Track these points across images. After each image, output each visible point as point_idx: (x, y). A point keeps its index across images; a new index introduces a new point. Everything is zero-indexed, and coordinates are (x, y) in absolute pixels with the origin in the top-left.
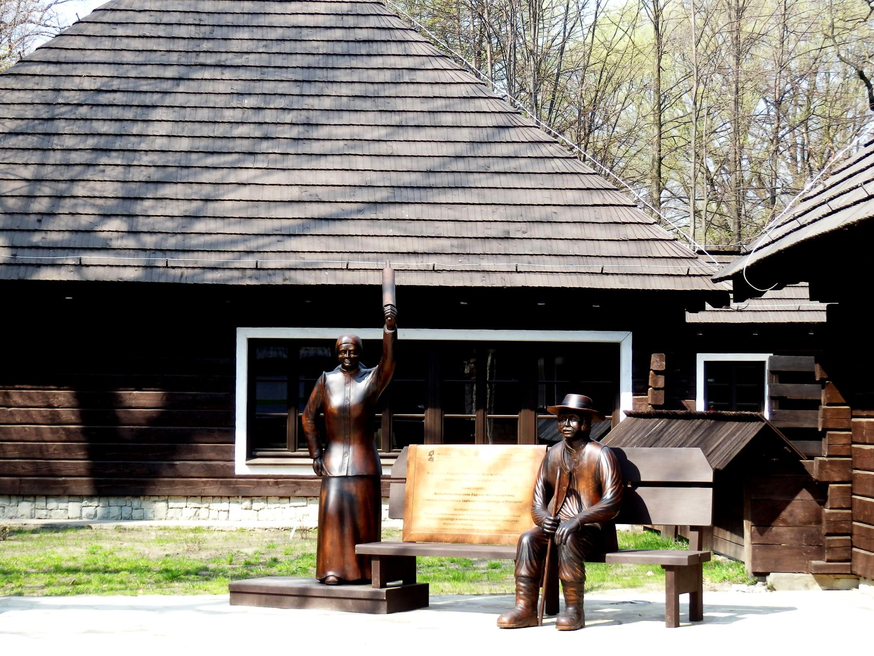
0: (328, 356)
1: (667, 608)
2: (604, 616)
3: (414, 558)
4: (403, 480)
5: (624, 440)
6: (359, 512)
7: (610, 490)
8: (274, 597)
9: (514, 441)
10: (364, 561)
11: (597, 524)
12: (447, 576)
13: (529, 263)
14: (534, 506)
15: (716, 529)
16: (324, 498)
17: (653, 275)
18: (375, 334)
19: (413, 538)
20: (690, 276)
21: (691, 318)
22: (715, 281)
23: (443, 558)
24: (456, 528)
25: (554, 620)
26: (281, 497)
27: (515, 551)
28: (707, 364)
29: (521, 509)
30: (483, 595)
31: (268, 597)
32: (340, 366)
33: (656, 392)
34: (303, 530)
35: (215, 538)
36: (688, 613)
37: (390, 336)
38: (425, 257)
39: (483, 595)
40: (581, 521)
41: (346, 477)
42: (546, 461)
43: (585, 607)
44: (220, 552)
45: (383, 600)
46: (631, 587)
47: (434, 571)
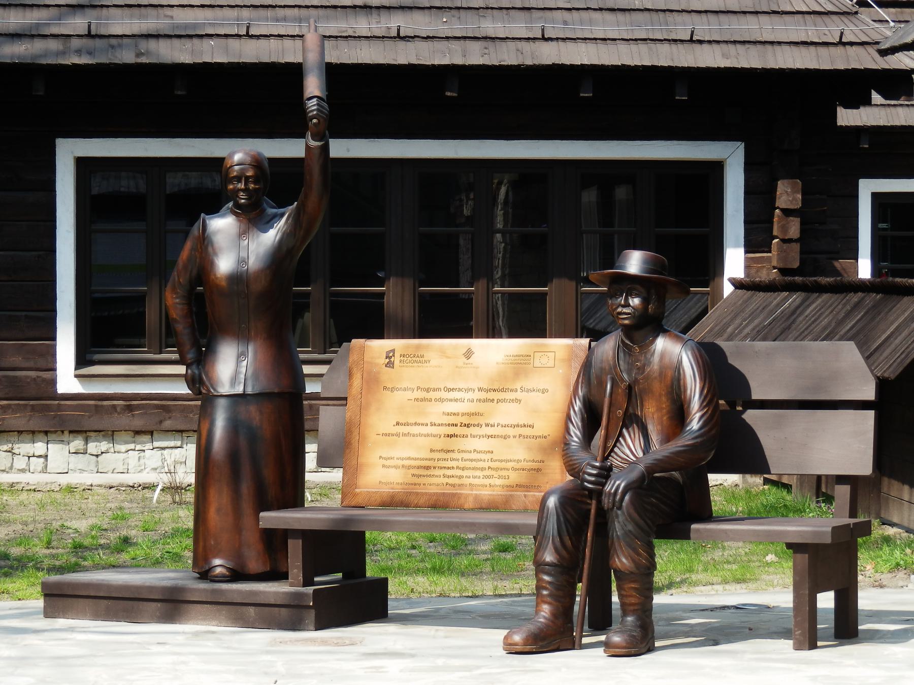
0: (207, 189)
1: (795, 616)
2: (690, 631)
3: (363, 534)
4: (342, 400)
5: (730, 330)
6: (263, 456)
7: (698, 415)
8: (123, 604)
9: (540, 332)
10: (274, 541)
11: (676, 474)
12: (421, 565)
13: (565, 23)
14: (566, 444)
15: (885, 481)
16: (204, 433)
17: (779, 43)
18: (291, 149)
19: (359, 500)
20: (845, 44)
21: (847, 117)
22: (884, 53)
23: (416, 535)
24: (436, 484)
25: (603, 638)
26: (137, 433)
27: (534, 521)
28: (876, 197)
29: (547, 450)
30: (483, 596)
31: (110, 602)
32: (231, 204)
33: (785, 246)
34: (174, 489)
35: (22, 504)
36: (832, 624)
37: (317, 152)
38: (384, 14)
39: (483, 596)
40: (647, 468)
41: (243, 396)
42: (587, 366)
43: (655, 617)
44: (31, 527)
45: (309, 607)
46: (738, 581)
47: (399, 557)
